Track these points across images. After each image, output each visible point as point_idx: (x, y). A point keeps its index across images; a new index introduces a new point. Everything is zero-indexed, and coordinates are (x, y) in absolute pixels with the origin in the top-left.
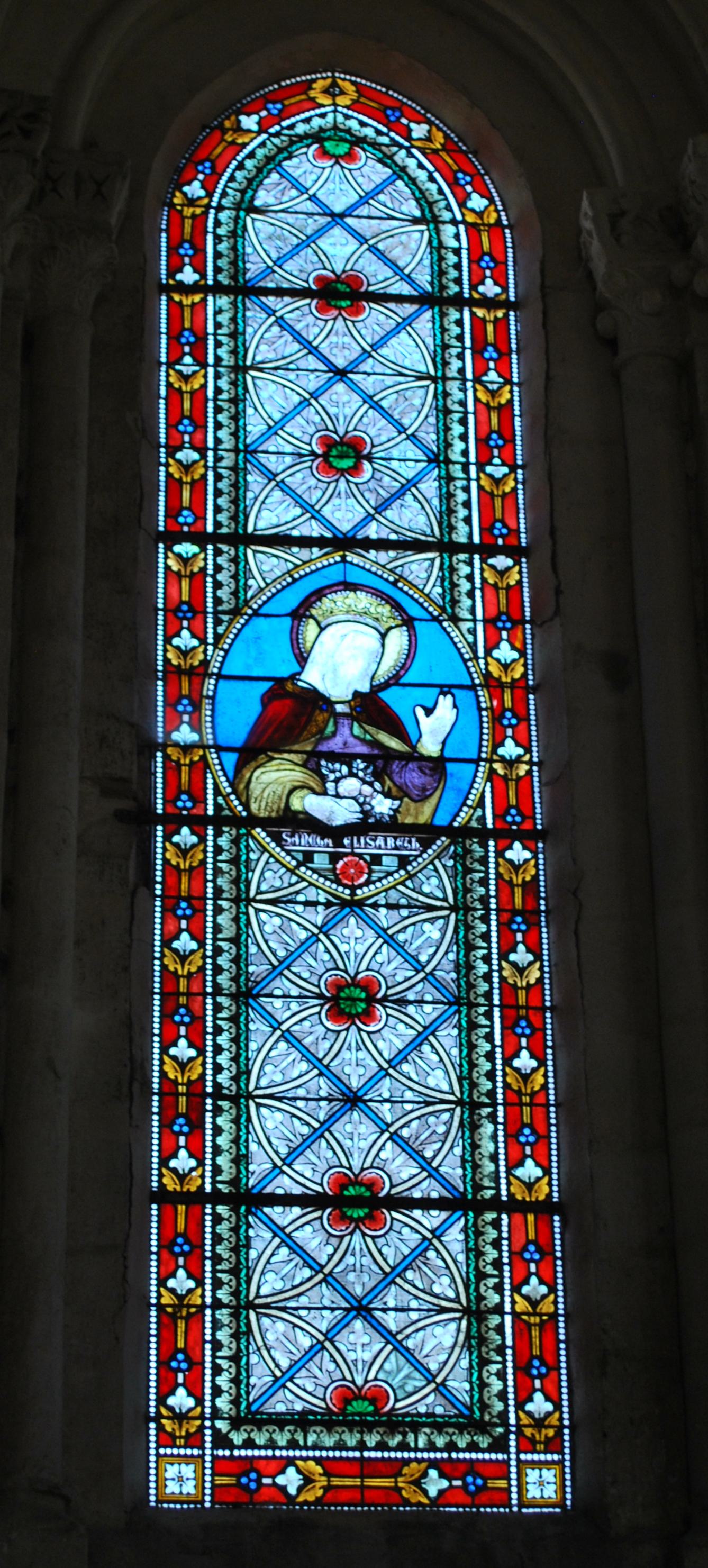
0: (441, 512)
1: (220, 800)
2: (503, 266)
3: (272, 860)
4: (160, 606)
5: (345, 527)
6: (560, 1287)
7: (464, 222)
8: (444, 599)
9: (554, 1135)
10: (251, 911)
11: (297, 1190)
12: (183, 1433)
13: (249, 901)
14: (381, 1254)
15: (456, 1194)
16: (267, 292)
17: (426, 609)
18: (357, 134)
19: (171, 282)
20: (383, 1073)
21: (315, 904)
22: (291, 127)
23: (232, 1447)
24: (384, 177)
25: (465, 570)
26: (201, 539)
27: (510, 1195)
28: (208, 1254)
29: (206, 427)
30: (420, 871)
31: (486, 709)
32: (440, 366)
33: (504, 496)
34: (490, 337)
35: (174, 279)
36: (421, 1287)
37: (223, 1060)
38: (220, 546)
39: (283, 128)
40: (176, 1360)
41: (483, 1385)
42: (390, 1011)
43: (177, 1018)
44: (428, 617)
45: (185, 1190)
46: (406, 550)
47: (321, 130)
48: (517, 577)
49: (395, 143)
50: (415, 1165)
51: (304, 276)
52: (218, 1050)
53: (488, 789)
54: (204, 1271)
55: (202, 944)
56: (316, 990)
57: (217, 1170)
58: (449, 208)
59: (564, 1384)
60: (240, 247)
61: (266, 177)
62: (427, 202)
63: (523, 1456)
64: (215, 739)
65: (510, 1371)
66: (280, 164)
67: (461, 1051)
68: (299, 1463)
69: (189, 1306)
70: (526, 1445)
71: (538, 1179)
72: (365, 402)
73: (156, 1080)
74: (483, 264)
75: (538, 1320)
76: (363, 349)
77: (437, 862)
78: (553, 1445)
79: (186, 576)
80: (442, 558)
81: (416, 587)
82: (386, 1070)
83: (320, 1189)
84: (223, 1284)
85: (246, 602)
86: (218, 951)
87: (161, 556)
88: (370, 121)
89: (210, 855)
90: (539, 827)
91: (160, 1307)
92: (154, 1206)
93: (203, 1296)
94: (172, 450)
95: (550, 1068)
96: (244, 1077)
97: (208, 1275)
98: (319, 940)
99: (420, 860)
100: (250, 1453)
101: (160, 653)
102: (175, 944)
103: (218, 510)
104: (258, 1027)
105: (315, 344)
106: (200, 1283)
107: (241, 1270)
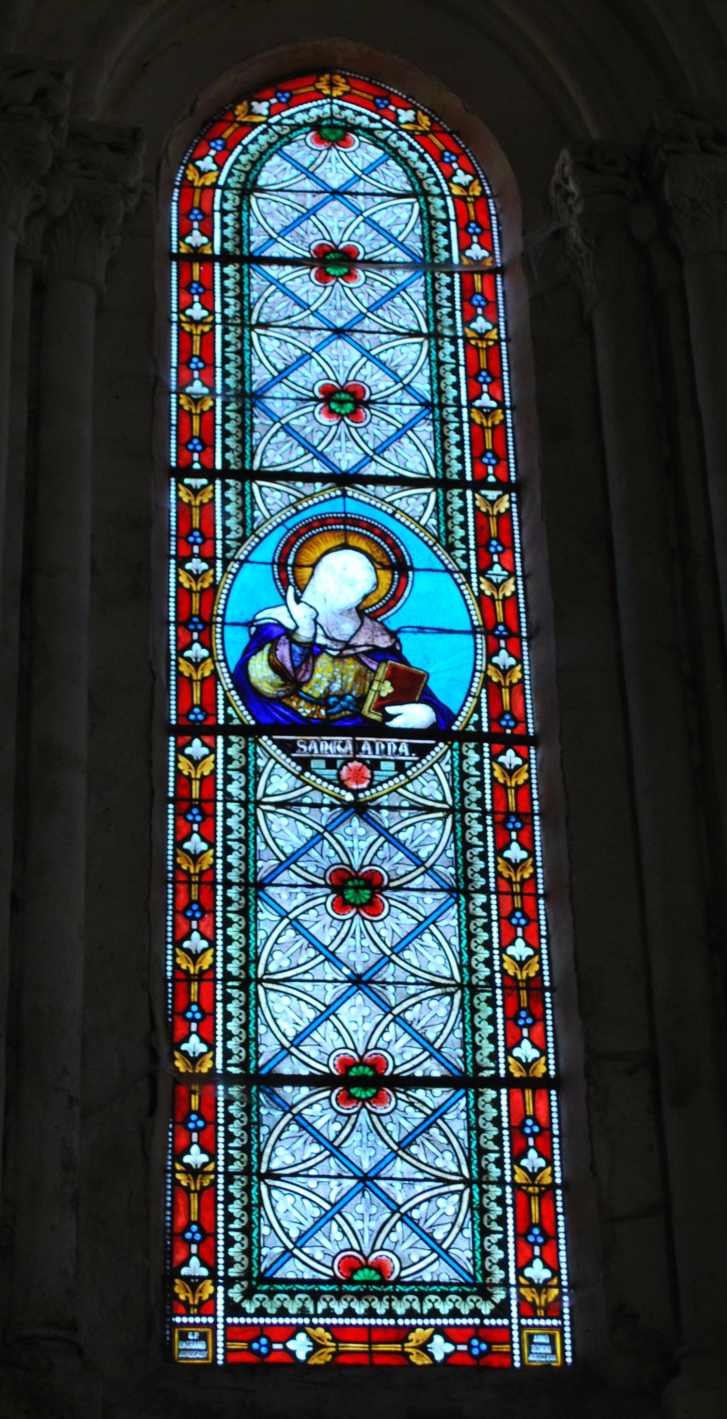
0: (469, 1149)
1: (230, 711)
2: (505, 463)
3: (278, 766)
4: (172, 619)
5: (344, 467)
6: (551, 1050)
7: (451, 195)
8: (438, 529)
9: (549, 1017)
10: (260, 814)
11: (304, 1071)
12: (196, 1302)
13: (258, 803)
14: (386, 1131)
15: (455, 1072)
18: (352, 122)
20: (386, 959)
21: (320, 806)
22: (291, 117)
23: (243, 1313)
24: (377, 157)
25: (474, 758)
26: (209, 473)
27: (508, 1072)
29: (214, 447)
30: (420, 775)
31: (480, 671)
32: (432, 323)
33: (512, 686)
34: (483, 364)
36: (425, 1161)
37: (233, 949)
38: (227, 481)
39: (283, 118)
40: (193, 713)
41: (485, 1254)
42: (362, 138)
43: (189, 1015)
45: (197, 1071)
46: (403, 485)
47: (320, 119)
48: (513, 588)
49: (386, 128)
50: (418, 1045)
51: (310, 386)
52: (228, 940)
53: (483, 695)
54: (216, 1035)
55: (212, 845)
56: (311, 394)
57: (228, 1054)
58: (437, 184)
59: (550, 1034)
60: (244, 219)
61: (267, 160)
62: (417, 178)
63: (523, 1322)
65: (511, 1239)
66: (280, 149)
67: (460, 942)
70: (528, 1310)
71: (535, 1060)
72: (363, 356)
73: (169, 968)
74: (481, 379)
75: (537, 1190)
76: (366, 453)
77: (436, 766)
78: (553, 1310)
79: (196, 779)
80: (437, 493)
81: (412, 518)
82: (389, 957)
83: (326, 1070)
85: (253, 531)
86: (228, 850)
87: (173, 488)
88: (363, 110)
95: (545, 957)
96: (252, 966)
97: (221, 1151)
98: (324, 838)
99: (419, 765)
100: (262, 1320)
101: (172, 764)
102: (187, 845)
103: (226, 449)
104: (266, 916)
105: (331, 948)
106: (213, 1158)
107: (253, 1229)
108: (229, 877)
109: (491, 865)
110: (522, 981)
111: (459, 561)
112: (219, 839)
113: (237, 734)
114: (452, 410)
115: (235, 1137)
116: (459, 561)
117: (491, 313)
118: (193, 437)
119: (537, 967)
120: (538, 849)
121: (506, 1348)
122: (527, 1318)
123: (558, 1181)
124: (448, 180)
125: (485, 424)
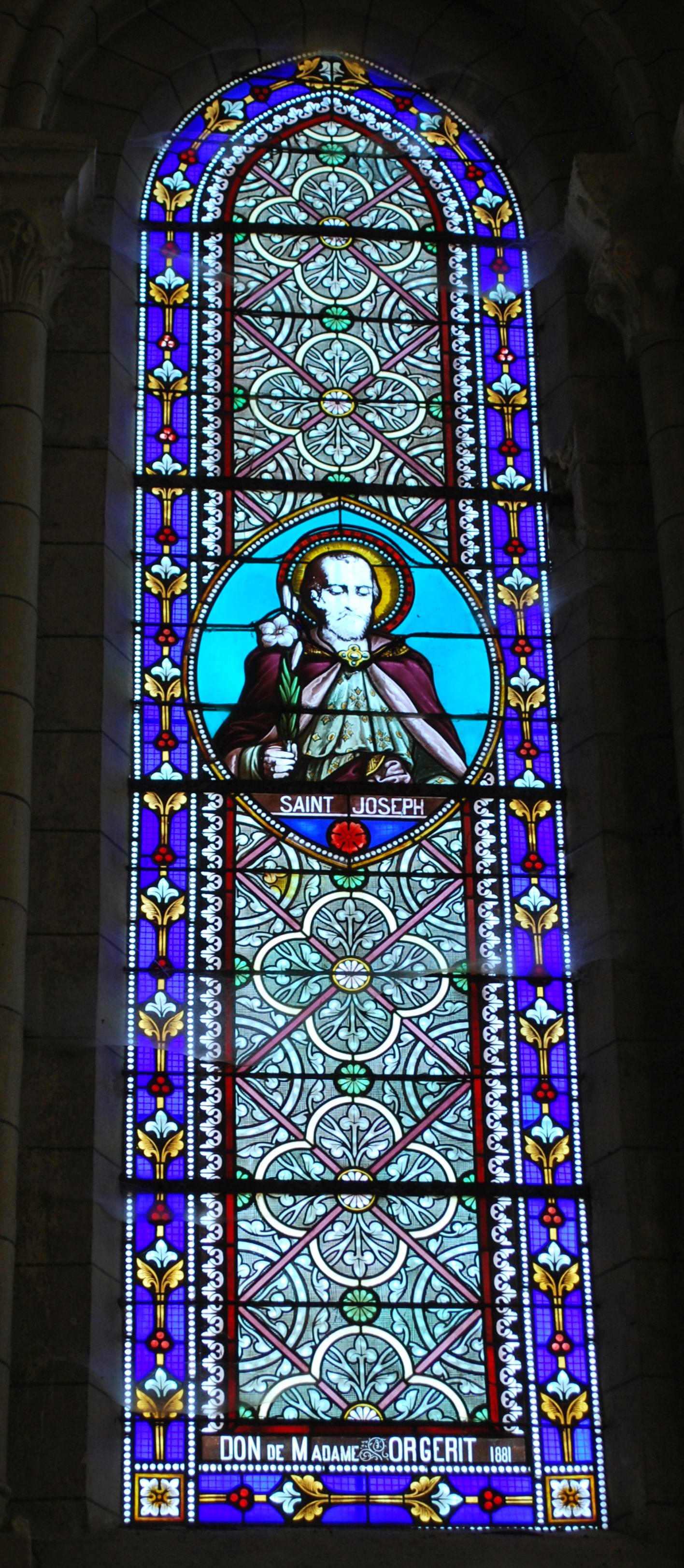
16: (261, 485)
25: (472, 514)
28: (193, 836)
35: (151, 468)
38: (207, 491)
44: (430, 562)
68: (296, 1478)
69: (175, 392)
84: (209, 904)
90: (579, 1182)
91: (148, 391)
93: (188, 384)
94: (150, 559)
110: (525, 712)
111: (474, 583)
113: (215, 791)
116: (474, 583)
117: (514, 282)
118: (164, 333)
119: (566, 1150)
120: (594, 1382)
124: (472, 201)
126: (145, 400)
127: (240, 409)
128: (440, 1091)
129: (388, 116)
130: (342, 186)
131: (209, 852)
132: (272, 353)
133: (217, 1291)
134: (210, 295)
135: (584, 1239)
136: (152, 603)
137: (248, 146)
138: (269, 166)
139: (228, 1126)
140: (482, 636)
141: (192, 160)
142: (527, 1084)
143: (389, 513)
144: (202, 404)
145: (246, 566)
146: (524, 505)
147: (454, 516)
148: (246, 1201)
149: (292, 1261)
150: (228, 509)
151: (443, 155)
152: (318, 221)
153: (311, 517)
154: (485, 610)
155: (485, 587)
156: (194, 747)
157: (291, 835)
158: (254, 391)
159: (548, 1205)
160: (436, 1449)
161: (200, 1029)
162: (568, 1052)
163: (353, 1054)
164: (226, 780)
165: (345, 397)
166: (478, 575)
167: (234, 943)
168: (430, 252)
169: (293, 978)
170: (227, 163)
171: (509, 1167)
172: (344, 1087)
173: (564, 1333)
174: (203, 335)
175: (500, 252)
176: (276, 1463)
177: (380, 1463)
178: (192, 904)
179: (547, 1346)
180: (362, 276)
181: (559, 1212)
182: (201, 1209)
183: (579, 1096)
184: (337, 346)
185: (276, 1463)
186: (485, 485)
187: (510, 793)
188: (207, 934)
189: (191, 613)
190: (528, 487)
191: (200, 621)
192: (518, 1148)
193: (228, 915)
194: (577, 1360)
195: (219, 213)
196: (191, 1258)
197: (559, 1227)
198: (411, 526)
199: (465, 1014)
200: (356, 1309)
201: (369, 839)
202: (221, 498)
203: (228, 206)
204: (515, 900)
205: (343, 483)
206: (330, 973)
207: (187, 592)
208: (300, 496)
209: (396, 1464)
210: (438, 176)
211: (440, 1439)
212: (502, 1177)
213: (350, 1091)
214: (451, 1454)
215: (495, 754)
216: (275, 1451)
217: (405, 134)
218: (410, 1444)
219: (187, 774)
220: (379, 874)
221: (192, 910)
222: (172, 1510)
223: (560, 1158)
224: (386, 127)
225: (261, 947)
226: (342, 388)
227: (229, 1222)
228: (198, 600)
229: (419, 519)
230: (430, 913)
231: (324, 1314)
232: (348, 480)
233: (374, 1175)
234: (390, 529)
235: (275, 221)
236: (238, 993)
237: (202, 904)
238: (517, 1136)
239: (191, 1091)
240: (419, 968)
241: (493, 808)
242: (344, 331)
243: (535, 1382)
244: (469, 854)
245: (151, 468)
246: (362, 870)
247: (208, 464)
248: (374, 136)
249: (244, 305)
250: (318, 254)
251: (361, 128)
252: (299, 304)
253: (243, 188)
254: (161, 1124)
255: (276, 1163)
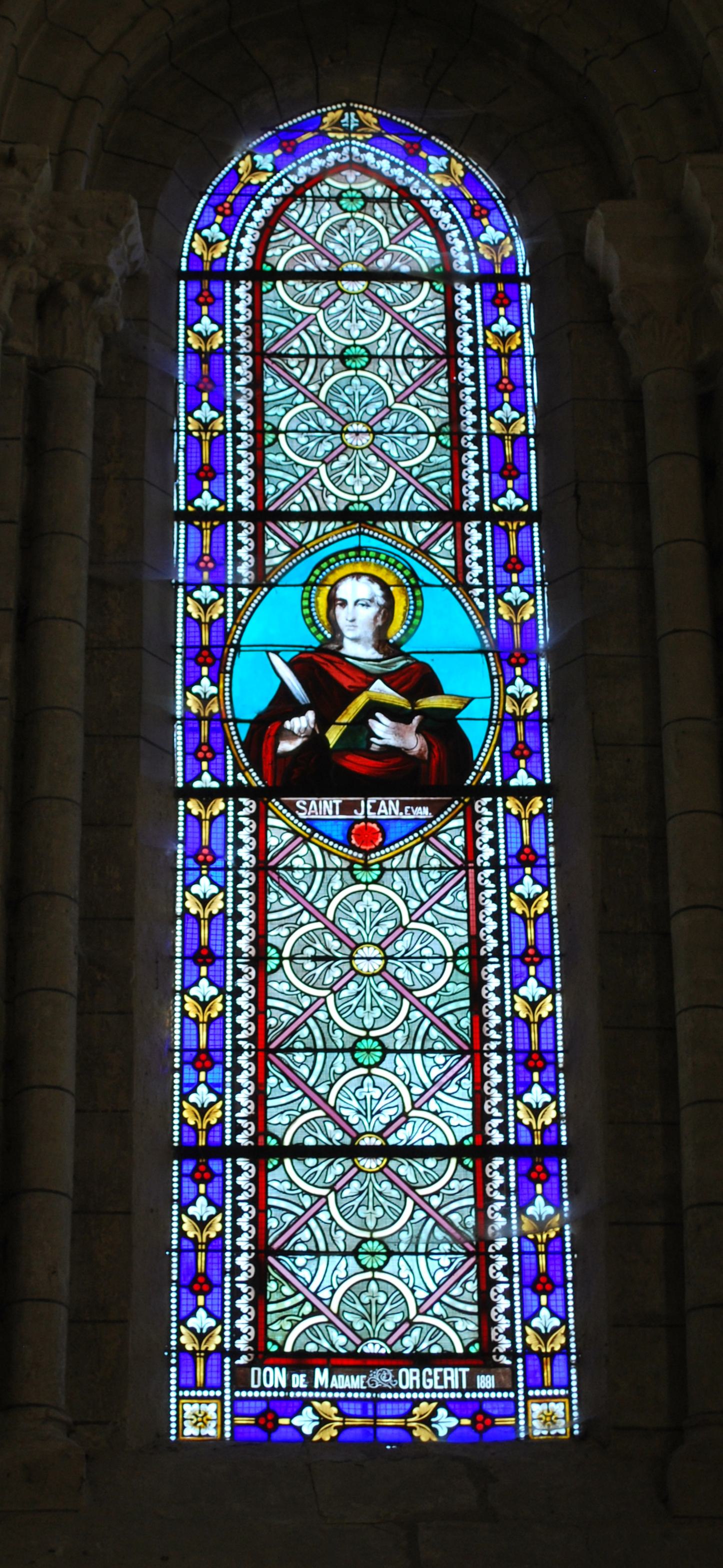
16: (290, 516)
17: (439, 578)
19: (190, 509)
25: (476, 536)
35: (193, 506)
38: (241, 800)
44: (440, 583)
64: (233, 714)
69: (212, 431)
89: (228, 1114)
91: (188, 433)
92: (176, 1162)
93: (224, 423)
94: (191, 587)
108: (237, 1346)
109: (492, 606)
111: (477, 600)
112: (228, 321)
114: (488, 873)
115: (242, 1029)
116: (477, 600)
121: (511, 1421)
122: (534, 1389)
123: (531, 431)
125: (543, 1350)
126: (186, 440)
127: (273, 971)
128: (440, 878)
129: (402, 163)
130: (364, 391)
131: (244, 853)
132: (296, 233)
133: (250, 1241)
134: (241, 340)
135: (551, 840)
136: (192, 625)
137: (276, 197)
138: (295, 215)
139: (260, 1097)
140: (484, 652)
141: (228, 212)
142: (521, 1057)
143: (403, 538)
144: (237, 441)
145: (273, 590)
146: (522, 524)
147: (461, 538)
148: (269, 287)
149: (314, 1216)
150: (258, 538)
151: (450, 198)
152: (338, 267)
153: (334, 542)
154: (486, 626)
155: (487, 604)
156: (230, 757)
157: (316, 835)
158: (282, 427)
159: (534, 1164)
160: (437, 1378)
161: (237, 1010)
162: (555, 1024)
163: (368, 1030)
164: (259, 787)
165: (364, 429)
166: (489, 803)
167: (266, 932)
168: (438, 292)
169: (319, 963)
170: (258, 215)
171: (503, 1128)
172: (358, 877)
173: (509, 378)
174: (236, 377)
175: (501, 287)
176: (302, 1390)
177: (393, 1391)
178: (227, 1333)
179: (496, 386)
180: (394, 1002)
181: (545, 1170)
182: (237, 1171)
183: (562, 988)
184: (358, 489)
185: (302, 1390)
186: (512, 1161)
187: (507, 791)
188: (243, 483)
189: (226, 635)
190: (525, 508)
191: (235, 642)
192: (511, 1113)
193: (260, 908)
194: (530, 670)
195: (251, 263)
196: (229, 1213)
197: (537, 965)
198: (422, 550)
199: (467, 994)
200: (369, 1257)
201: (384, 837)
202: (252, 528)
203: (259, 255)
204: (510, 888)
205: (362, 512)
206: (351, 958)
207: (223, 616)
208: (323, 525)
209: (405, 1391)
210: (446, 217)
211: (440, 1370)
212: (497, 1138)
213: (366, 1063)
214: (449, 1382)
215: (493, 757)
216: (299, 1380)
217: (417, 178)
218: (415, 1374)
219: (223, 782)
220: (393, 870)
221: (227, 1339)
222: (211, 1431)
223: (545, 1014)
224: (399, 173)
225: (289, 936)
226: (357, 261)
227: (260, 1181)
228: (234, 623)
229: (444, 1079)
230: (415, 229)
231: (327, 206)
232: (366, 508)
233: (385, 1139)
234: (404, 552)
235: (299, 268)
236: (269, 978)
237: (238, 899)
238: (518, 1328)
239: (229, 1065)
240: (427, 952)
241: (492, 806)
242: (363, 368)
243: (486, 409)
244: (471, 851)
245: (193, 506)
246: (377, 866)
247: (243, 499)
248: (390, 183)
249: (273, 349)
250: (351, 980)
251: (378, 175)
252: (322, 345)
253: (273, 238)
254: (202, 1095)
255: (303, 1335)
